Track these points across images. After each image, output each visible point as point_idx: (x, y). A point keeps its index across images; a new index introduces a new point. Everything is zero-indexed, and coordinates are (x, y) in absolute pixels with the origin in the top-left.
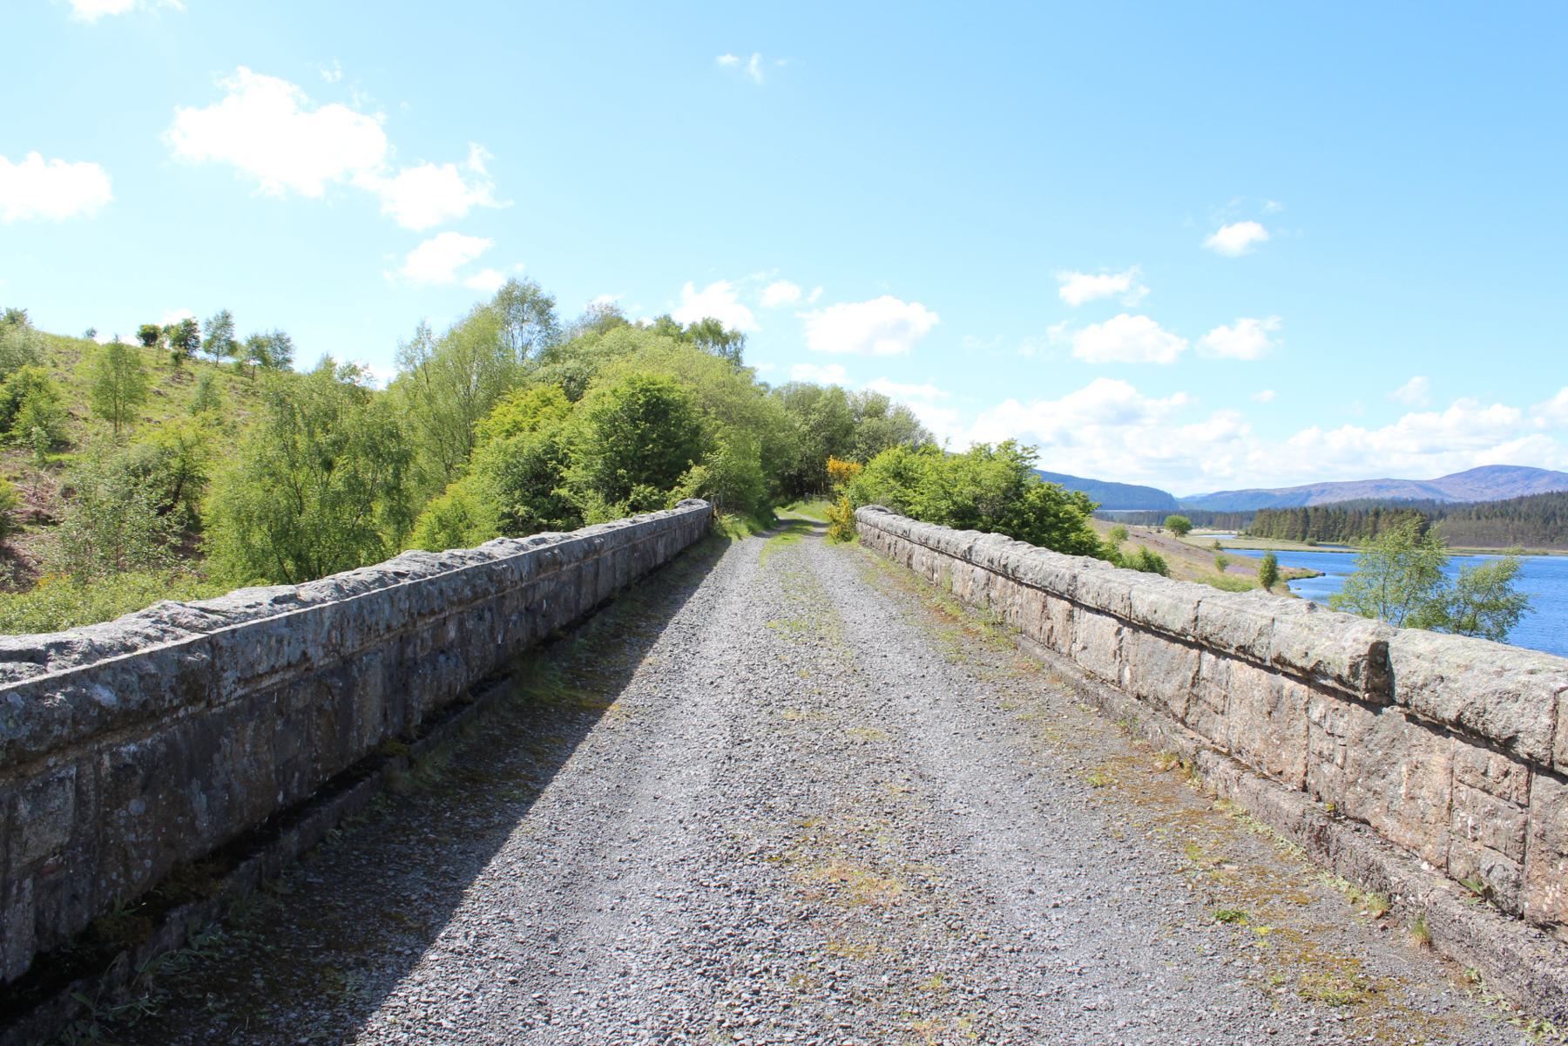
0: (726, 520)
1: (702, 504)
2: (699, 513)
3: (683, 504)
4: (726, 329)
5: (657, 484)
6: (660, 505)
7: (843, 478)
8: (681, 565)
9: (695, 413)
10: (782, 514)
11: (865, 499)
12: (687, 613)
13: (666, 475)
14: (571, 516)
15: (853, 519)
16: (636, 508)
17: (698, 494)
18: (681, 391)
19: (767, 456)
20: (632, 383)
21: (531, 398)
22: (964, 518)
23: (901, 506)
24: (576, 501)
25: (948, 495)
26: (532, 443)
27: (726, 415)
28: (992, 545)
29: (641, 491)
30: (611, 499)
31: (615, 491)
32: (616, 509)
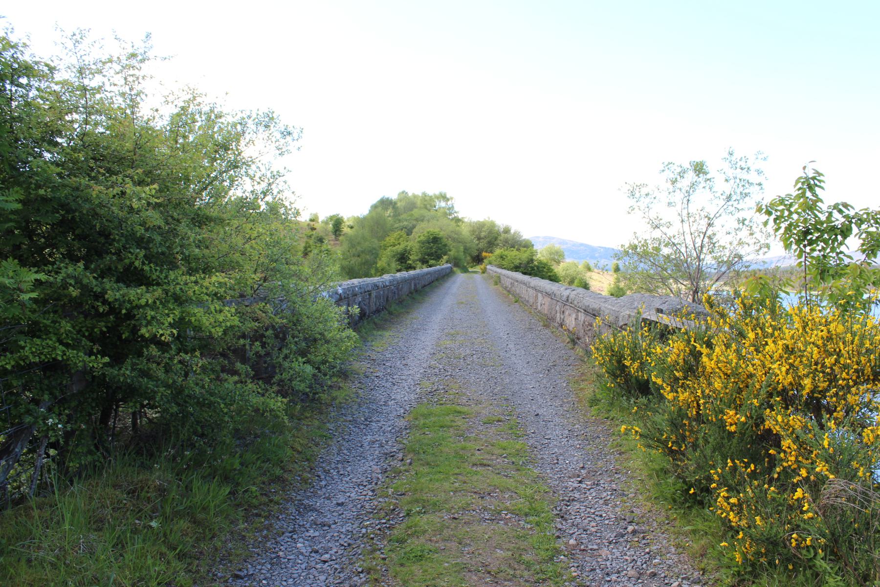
0: (455, 269)
1: (449, 265)
2: (447, 268)
3: (443, 265)
4: (448, 196)
5: (436, 260)
6: (435, 266)
7: (486, 257)
8: (436, 283)
9: (444, 241)
10: (470, 270)
11: (490, 263)
12: (447, 285)
13: (438, 257)
14: (410, 268)
15: (485, 268)
16: (431, 266)
17: (447, 262)
18: (442, 234)
19: (466, 250)
20: (428, 232)
21: (396, 235)
22: (516, 268)
23: (501, 266)
24: (414, 265)
25: (513, 263)
26: (399, 248)
27: (454, 240)
28: (519, 276)
29: (432, 262)
30: (423, 264)
31: (424, 261)
32: (424, 266)
